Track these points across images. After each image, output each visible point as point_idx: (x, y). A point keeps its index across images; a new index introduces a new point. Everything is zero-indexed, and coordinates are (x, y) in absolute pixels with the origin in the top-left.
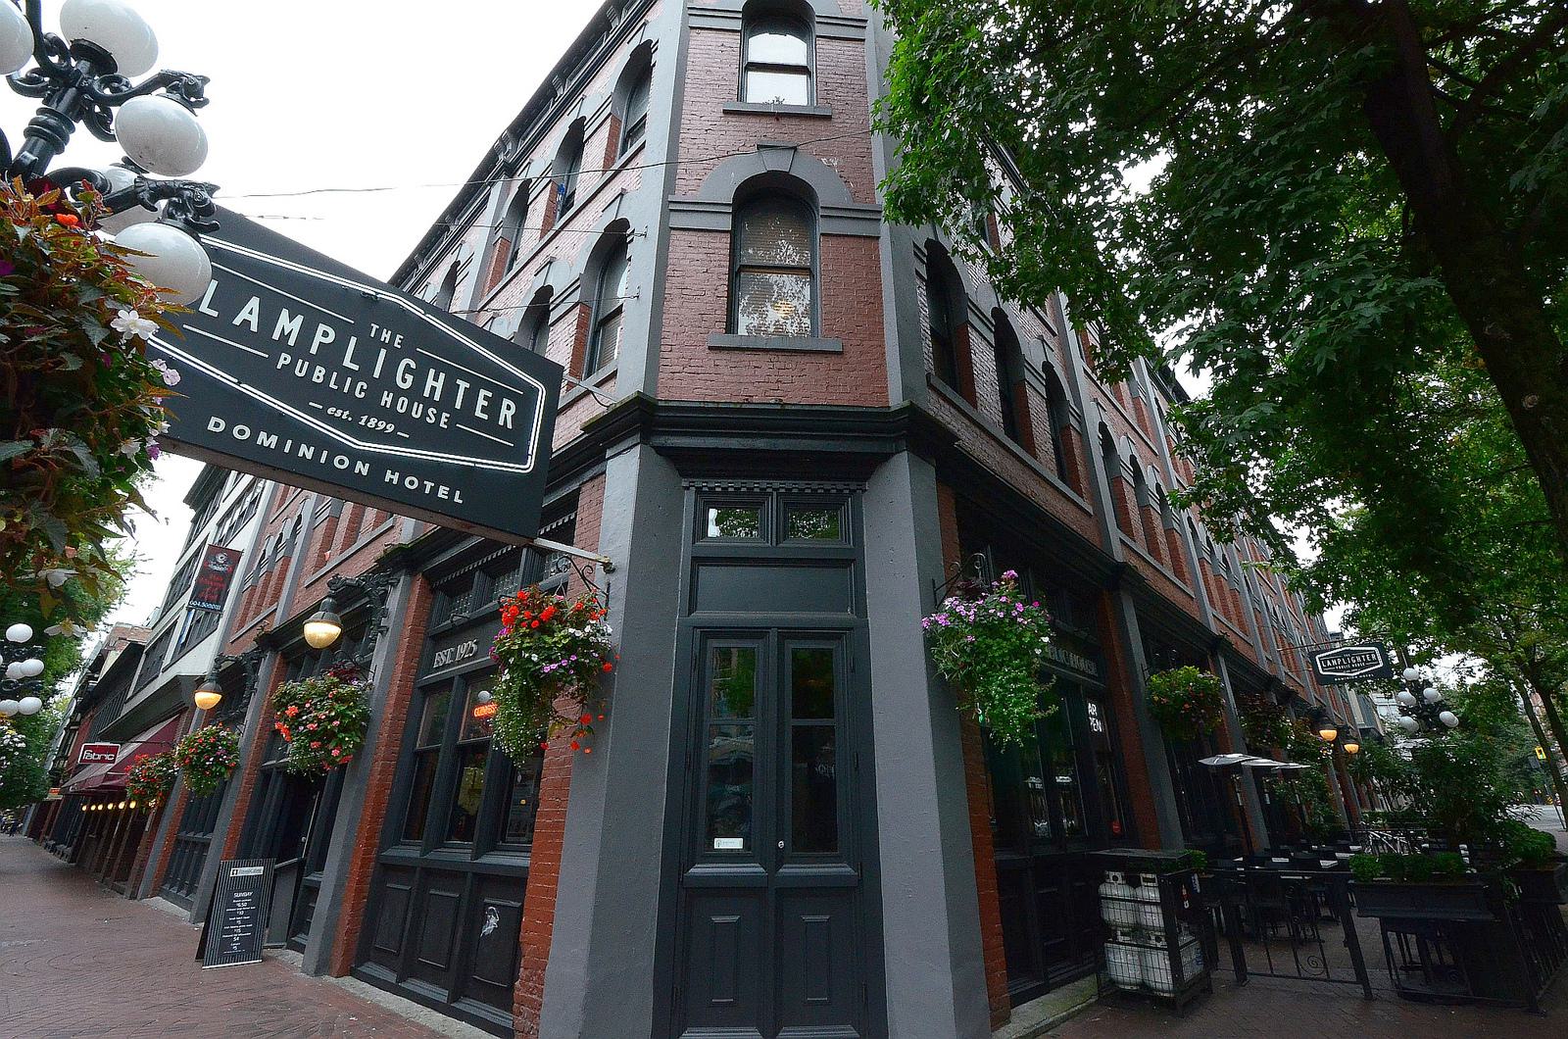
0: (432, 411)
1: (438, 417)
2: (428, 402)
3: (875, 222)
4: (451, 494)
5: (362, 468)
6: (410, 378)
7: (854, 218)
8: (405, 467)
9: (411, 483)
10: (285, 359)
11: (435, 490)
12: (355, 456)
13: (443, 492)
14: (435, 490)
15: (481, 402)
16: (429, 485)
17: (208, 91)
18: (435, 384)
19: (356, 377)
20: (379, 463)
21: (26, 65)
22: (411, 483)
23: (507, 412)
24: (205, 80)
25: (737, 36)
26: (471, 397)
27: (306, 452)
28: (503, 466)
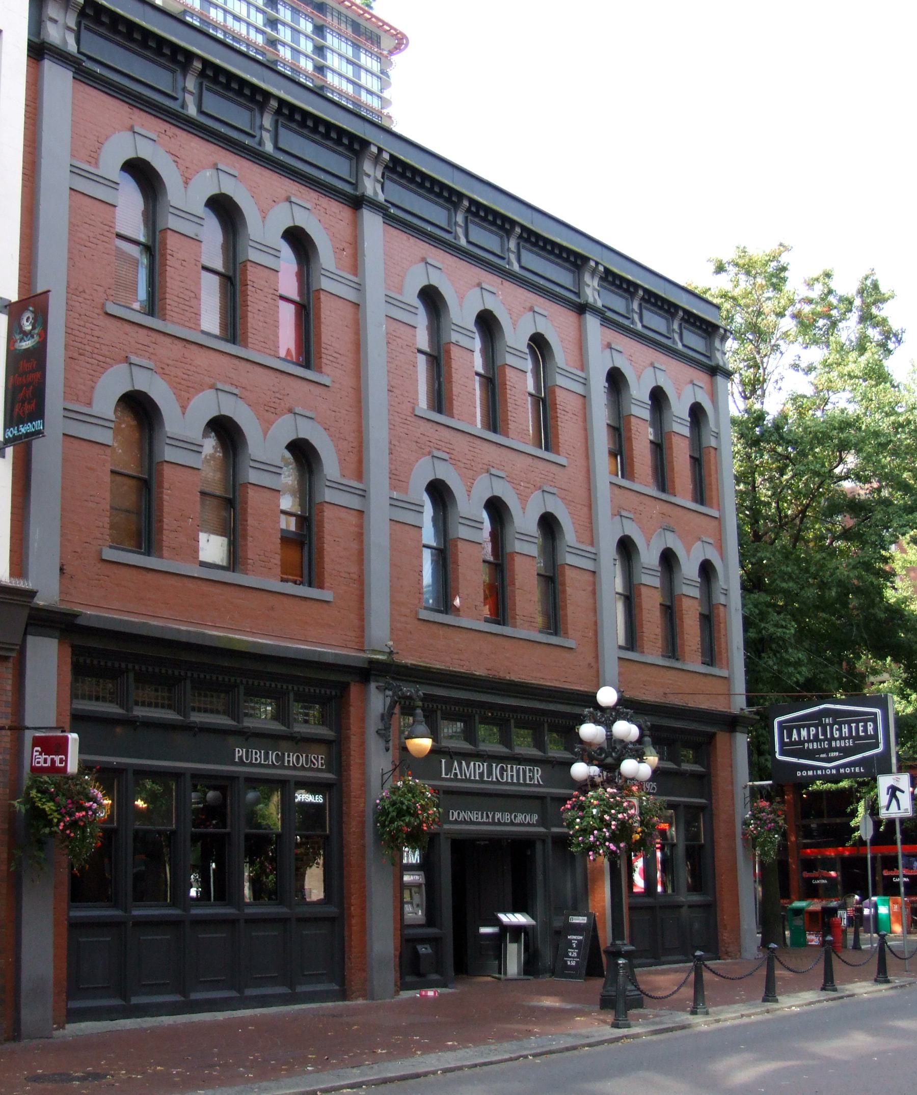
0: (838, 742)
1: (849, 742)
2: (845, 738)
3: (276, 475)
4: (860, 769)
5: (834, 771)
6: (838, 732)
7: (275, 473)
8: (844, 766)
9: (848, 770)
10: (806, 745)
11: (855, 770)
12: (831, 768)
13: (857, 770)
14: (855, 770)
15: (861, 729)
16: (853, 769)
17: (905, 337)
18: (845, 730)
19: (824, 740)
20: (837, 768)
21: (431, 524)
22: (848, 770)
23: (870, 727)
24: (788, 264)
25: (28, 723)
26: (857, 728)
27: (819, 772)
28: (11, 599)
